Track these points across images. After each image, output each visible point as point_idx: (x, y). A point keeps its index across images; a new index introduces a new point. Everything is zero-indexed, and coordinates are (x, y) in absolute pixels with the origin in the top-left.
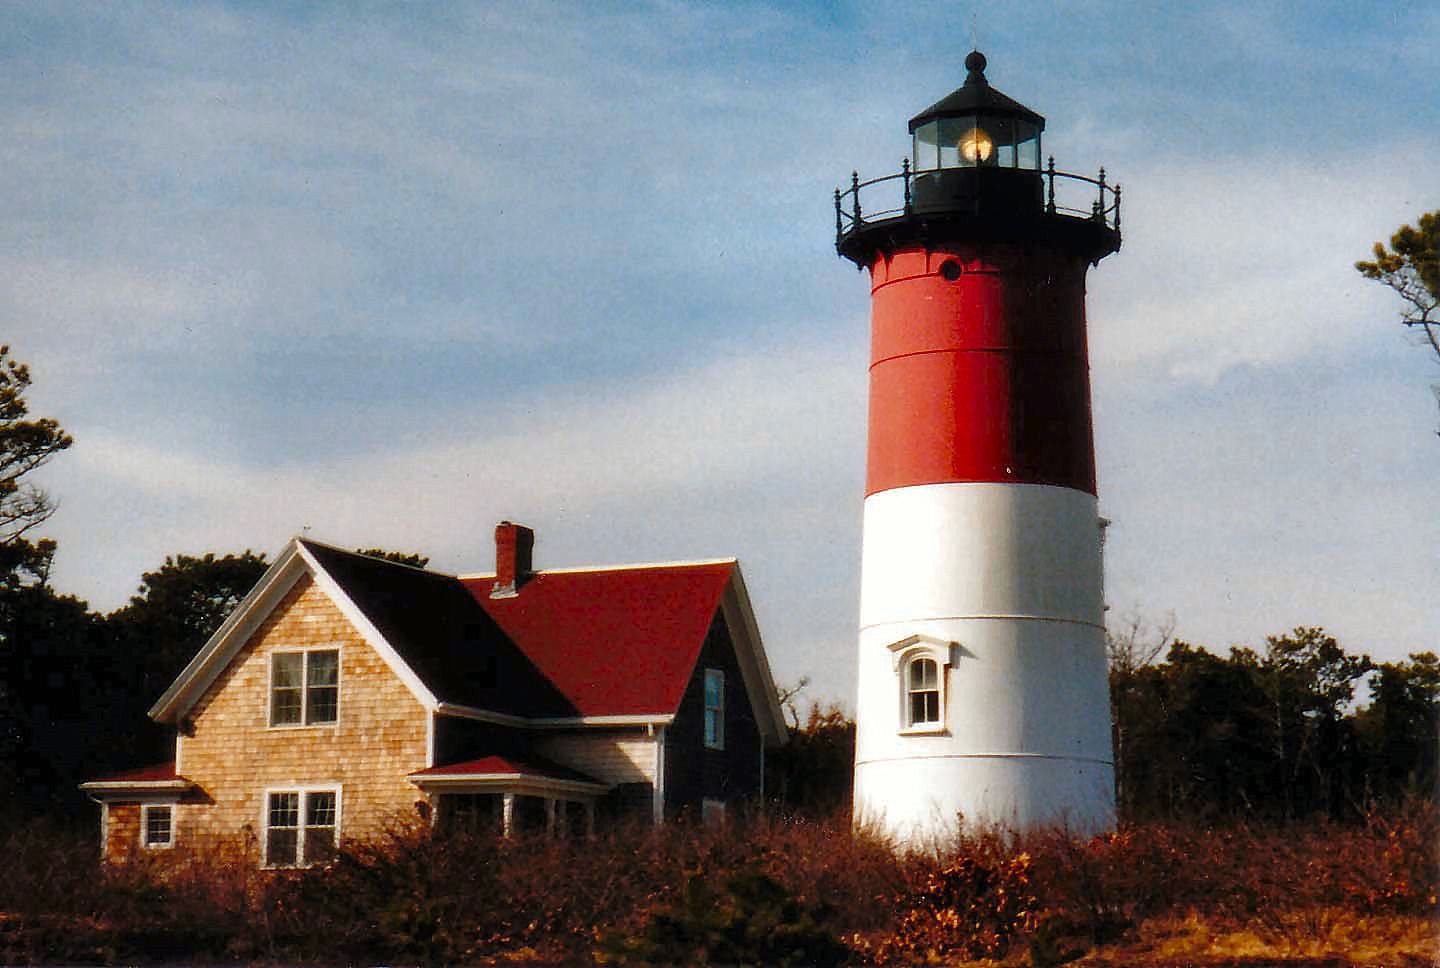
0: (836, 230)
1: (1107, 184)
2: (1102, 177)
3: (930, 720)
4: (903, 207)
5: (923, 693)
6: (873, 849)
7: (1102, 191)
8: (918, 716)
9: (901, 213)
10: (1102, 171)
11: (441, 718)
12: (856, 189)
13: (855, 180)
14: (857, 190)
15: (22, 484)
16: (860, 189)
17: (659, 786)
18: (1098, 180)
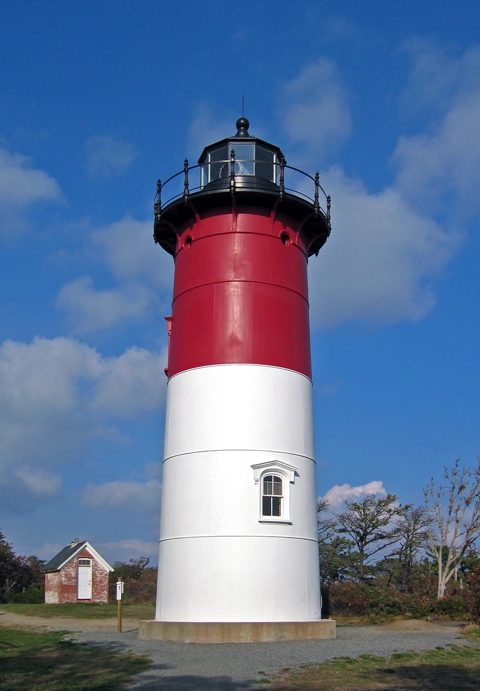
5: (271, 497)
8: (266, 512)
13: (186, 165)
14: (188, 171)
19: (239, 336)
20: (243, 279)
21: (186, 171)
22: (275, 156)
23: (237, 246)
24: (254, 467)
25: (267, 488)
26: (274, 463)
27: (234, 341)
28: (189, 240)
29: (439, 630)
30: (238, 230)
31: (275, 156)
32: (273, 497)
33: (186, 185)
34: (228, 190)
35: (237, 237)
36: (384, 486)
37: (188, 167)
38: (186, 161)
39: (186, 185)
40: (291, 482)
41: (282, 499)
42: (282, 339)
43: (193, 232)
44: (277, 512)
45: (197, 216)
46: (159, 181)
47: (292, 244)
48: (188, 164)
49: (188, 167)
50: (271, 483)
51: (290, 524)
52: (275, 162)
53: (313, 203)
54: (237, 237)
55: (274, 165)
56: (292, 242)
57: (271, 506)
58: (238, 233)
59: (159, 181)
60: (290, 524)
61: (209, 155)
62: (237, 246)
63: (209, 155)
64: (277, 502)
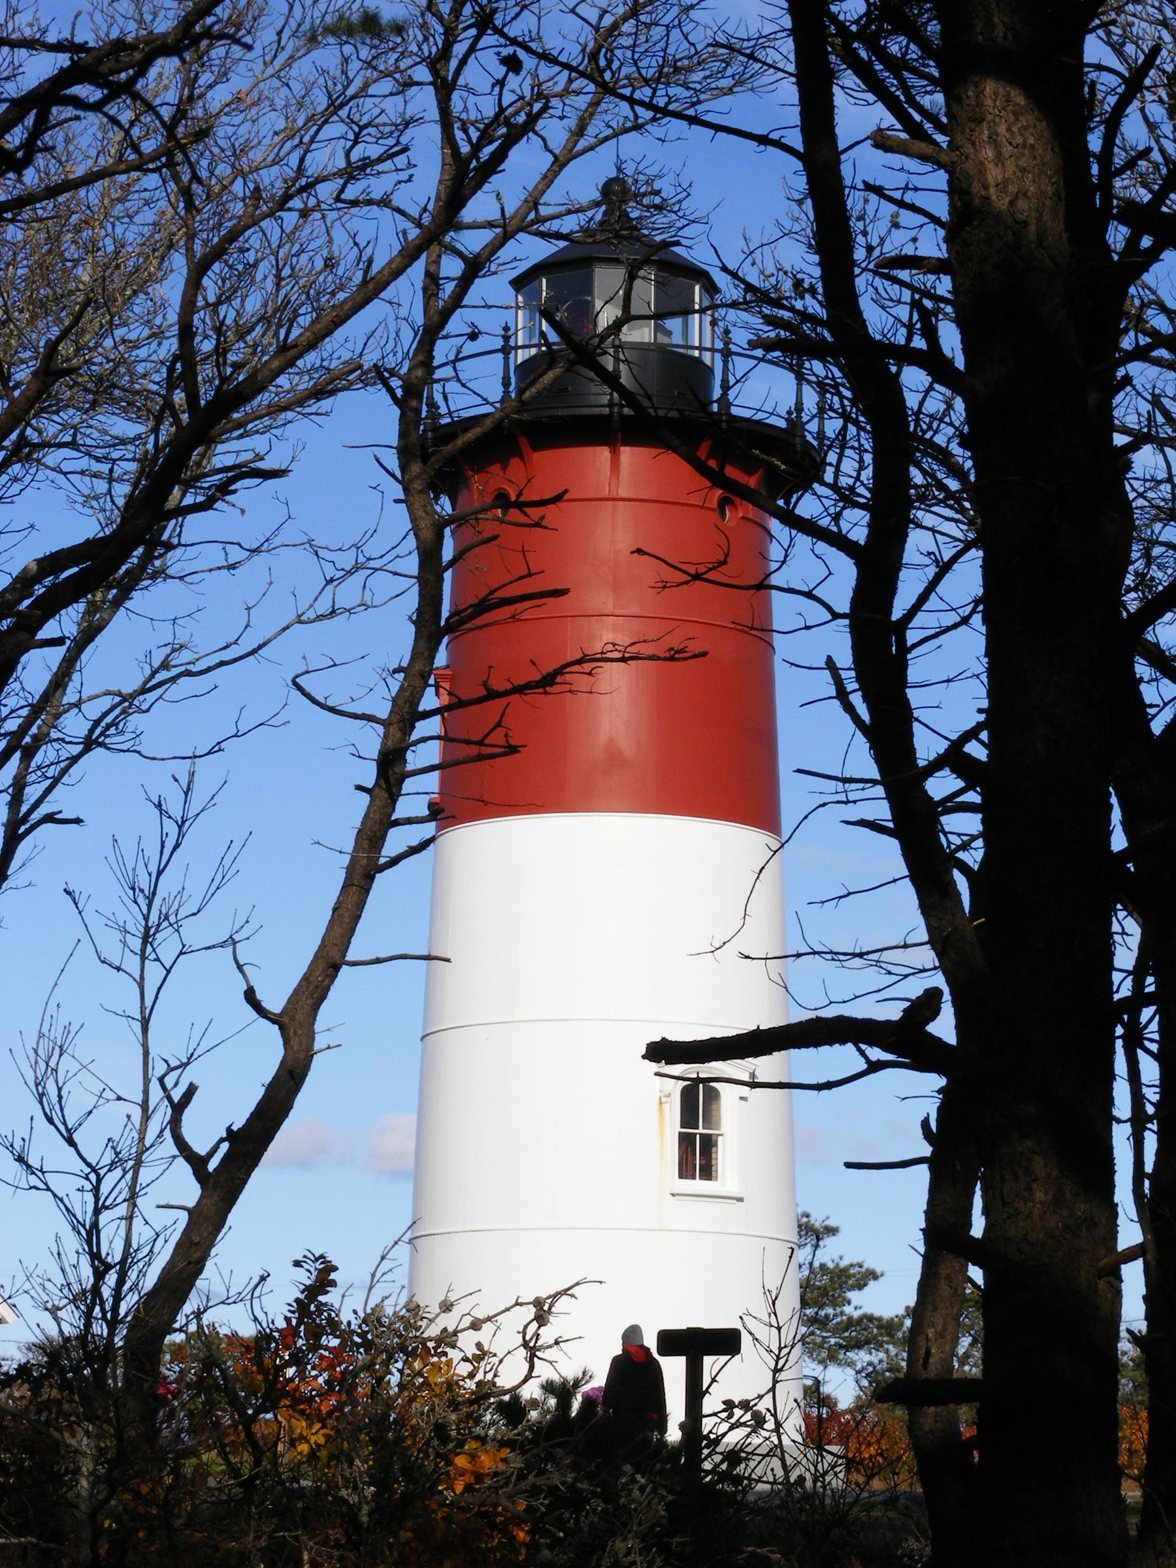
8: (686, 1171)
19: (627, 746)
20: (635, 610)
22: (697, 288)
25: (689, 1115)
27: (613, 757)
30: (623, 493)
31: (697, 288)
32: (701, 1135)
34: (606, 411)
36: (988, 756)
40: (741, 1098)
41: (720, 1139)
44: (708, 1173)
45: (524, 443)
46: (566, 491)
47: (743, 518)
51: (740, 1200)
56: (741, 515)
58: (623, 499)
59: (566, 491)
60: (740, 1200)
61: (544, 281)
63: (544, 281)
64: (709, 1143)
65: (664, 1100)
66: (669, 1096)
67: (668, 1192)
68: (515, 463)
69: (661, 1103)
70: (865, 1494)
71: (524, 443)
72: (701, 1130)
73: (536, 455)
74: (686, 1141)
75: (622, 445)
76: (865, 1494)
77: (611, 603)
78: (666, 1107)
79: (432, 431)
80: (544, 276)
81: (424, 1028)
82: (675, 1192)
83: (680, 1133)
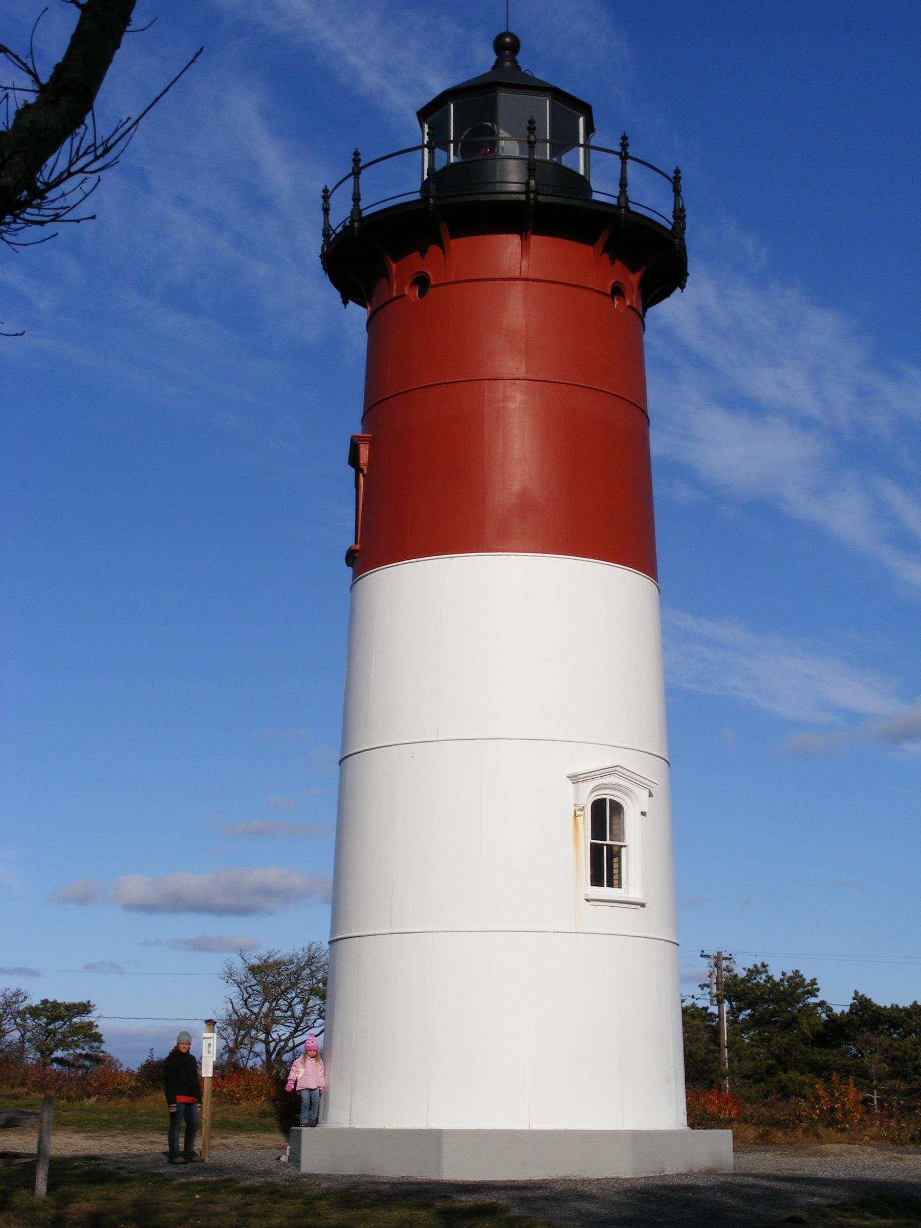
0: (352, 203)
1: (630, 154)
2: (624, 146)
3: (610, 885)
4: (419, 189)
5: (604, 845)
6: (118, 1080)
7: (624, 163)
8: (596, 880)
9: (417, 196)
10: (624, 138)
11: (693, 1017)
12: (356, 173)
13: (356, 161)
14: (359, 173)
15: (164, 1117)
16: (363, 171)
17: (822, 1196)
18: (619, 149)
21: (356, 173)
23: (516, 310)
24: (575, 779)
25: (598, 830)
26: (610, 771)
28: (422, 282)
29: (235, 1140)
32: (607, 845)
33: (356, 199)
35: (515, 286)
37: (361, 165)
38: (357, 154)
39: (356, 199)
40: (643, 814)
41: (623, 850)
42: (607, 508)
43: (430, 263)
45: (444, 230)
47: (630, 306)
48: (359, 160)
49: (361, 165)
50: (605, 816)
51: (643, 905)
52: (581, 141)
53: (670, 227)
54: (515, 286)
55: (582, 149)
56: (628, 303)
57: (604, 866)
60: (643, 905)
61: (452, 106)
62: (516, 310)
63: (452, 106)
64: (614, 854)
65: (578, 813)
66: (582, 809)
67: (583, 898)
68: (434, 249)
69: (575, 816)
70: (272, 1045)
71: (444, 230)
72: (608, 842)
73: (454, 242)
74: (596, 851)
75: (533, 234)
76: (272, 1045)
77: (523, 369)
78: (580, 819)
79: (358, 221)
80: (452, 101)
81: (343, 749)
82: (590, 897)
83: (591, 844)
